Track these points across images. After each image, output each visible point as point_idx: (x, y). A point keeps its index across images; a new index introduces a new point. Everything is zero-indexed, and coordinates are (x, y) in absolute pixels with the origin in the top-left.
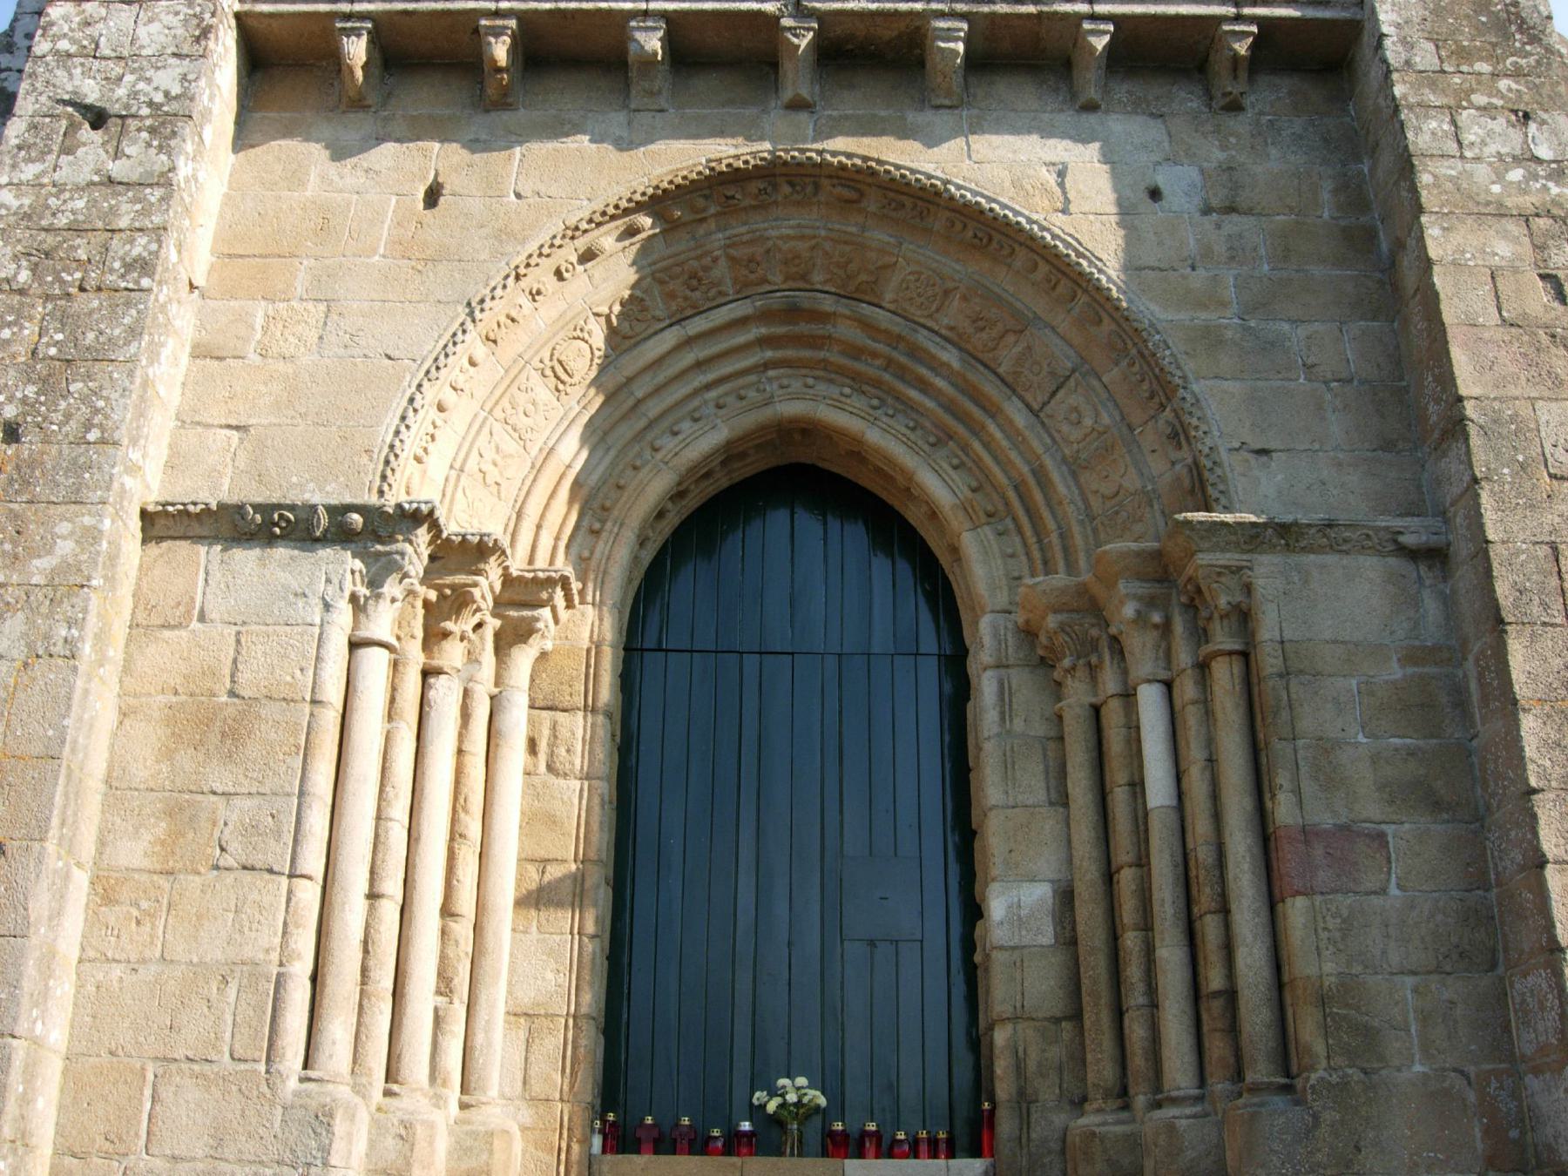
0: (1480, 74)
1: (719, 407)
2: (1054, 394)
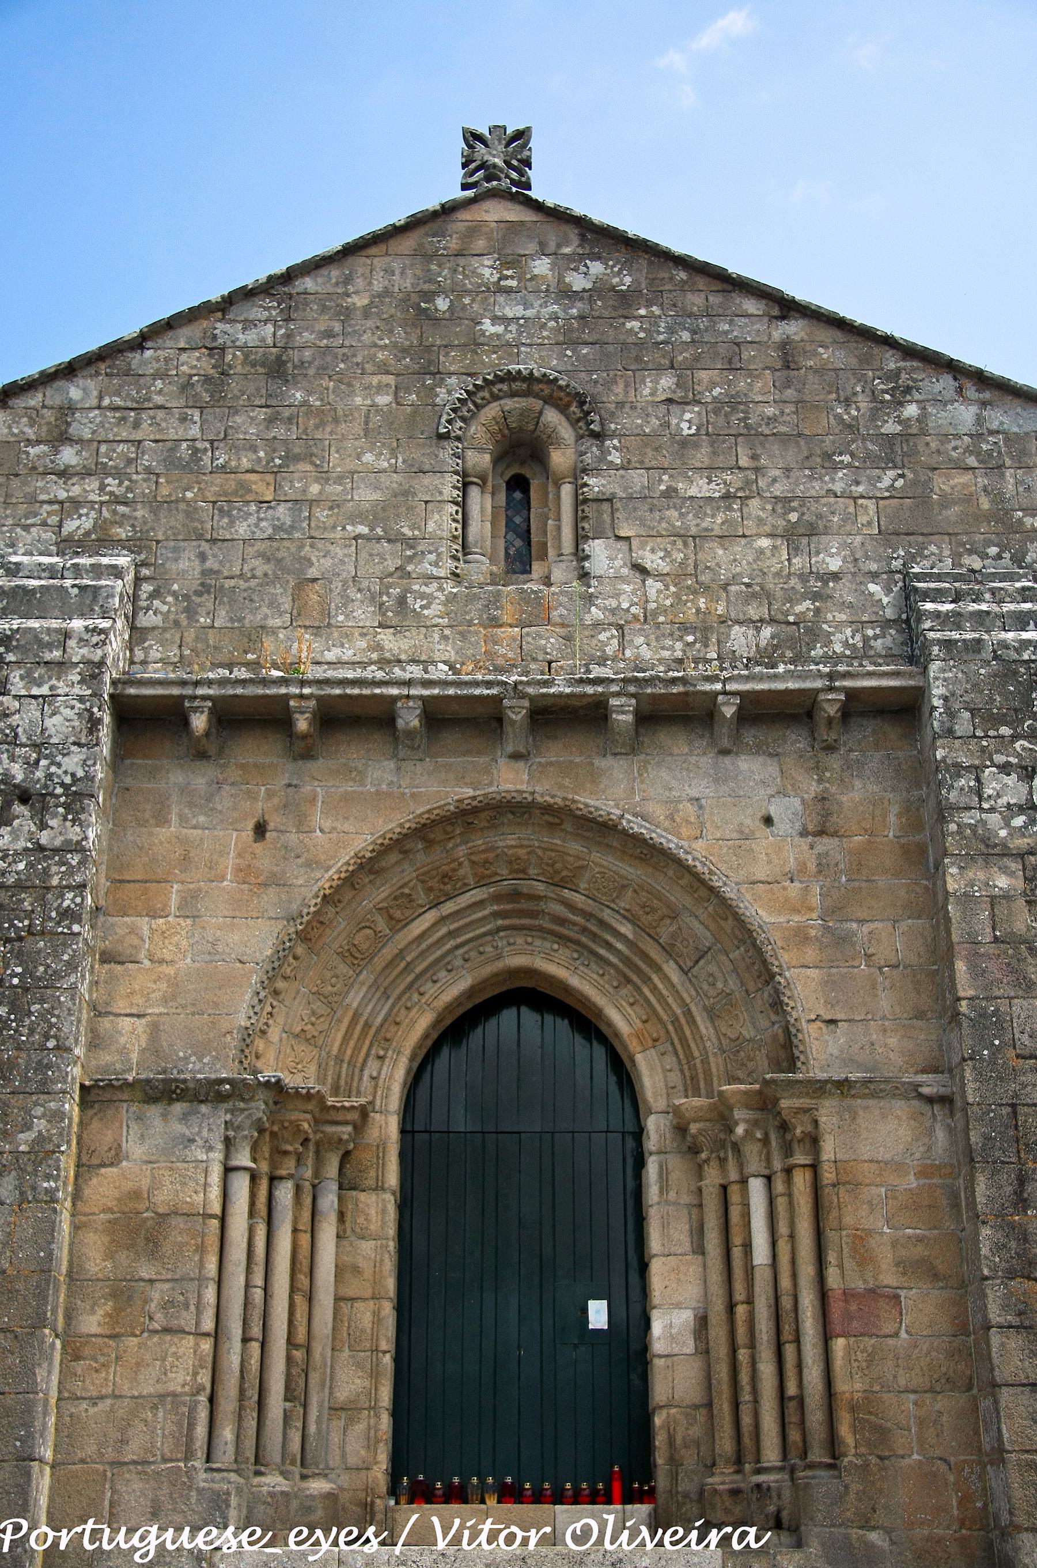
0: (1003, 737)
1: (466, 960)
2: (697, 962)
